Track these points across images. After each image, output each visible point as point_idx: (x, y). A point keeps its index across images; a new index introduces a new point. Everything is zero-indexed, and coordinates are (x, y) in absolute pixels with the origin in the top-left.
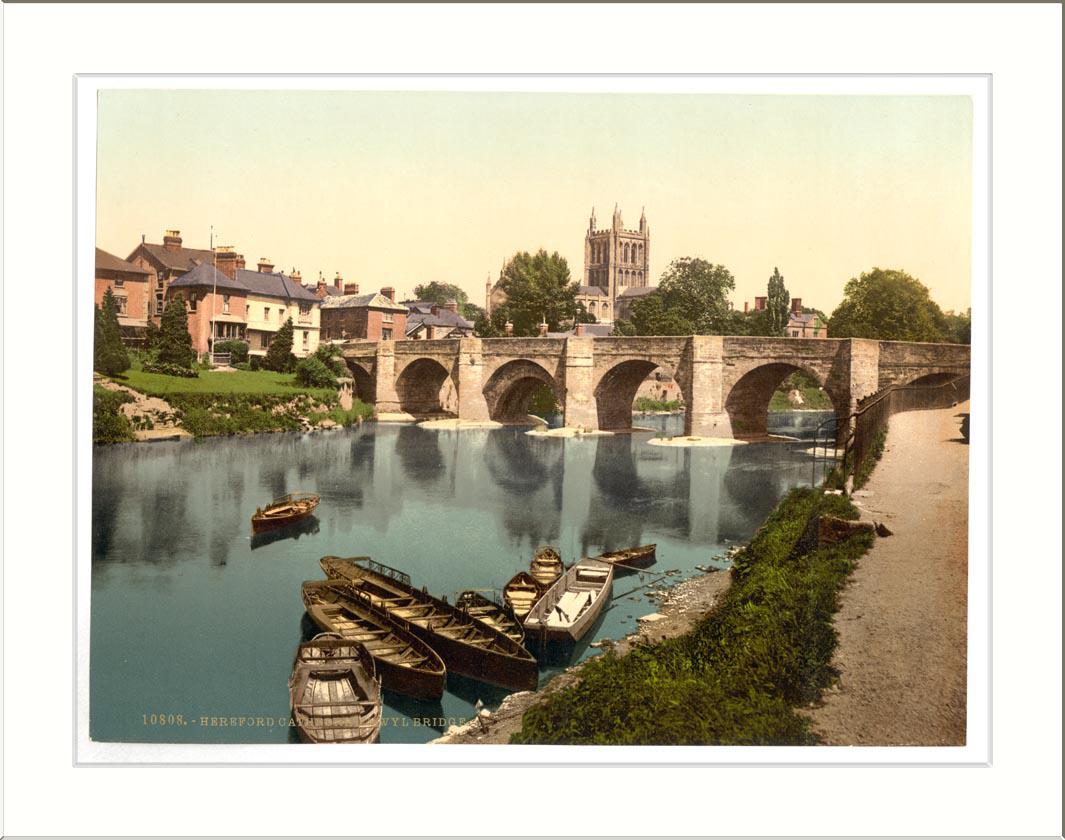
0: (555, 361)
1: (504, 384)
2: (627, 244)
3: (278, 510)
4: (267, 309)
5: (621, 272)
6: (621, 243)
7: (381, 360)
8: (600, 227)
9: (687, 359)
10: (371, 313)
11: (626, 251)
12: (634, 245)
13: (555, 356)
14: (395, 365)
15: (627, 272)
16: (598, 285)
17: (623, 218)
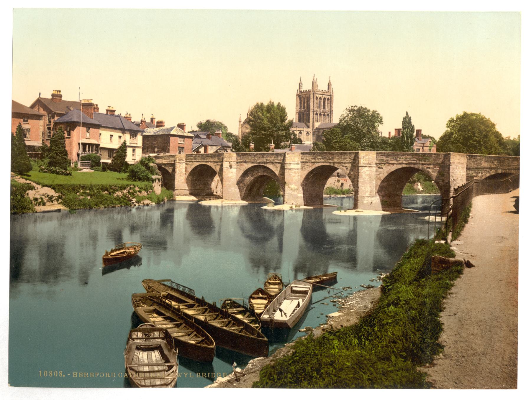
0: (279, 166)
1: (249, 179)
2: (320, 98)
4: (111, 136)
5: (317, 114)
7: (177, 165)
9: (355, 165)
11: (320, 102)
12: (325, 99)
13: (279, 163)
14: (186, 168)
15: (320, 114)
16: (303, 122)
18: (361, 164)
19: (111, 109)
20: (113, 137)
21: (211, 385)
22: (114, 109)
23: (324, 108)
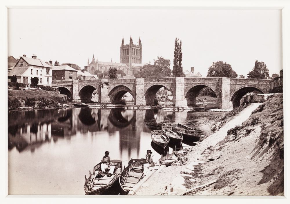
0: (132, 86)
1: (115, 92)
2: (135, 49)
3: (34, 91)
4: (37, 71)
5: (133, 58)
6: (133, 49)
7: (74, 86)
8: (125, 44)
9: (174, 85)
10: (66, 72)
11: (134, 51)
12: (137, 49)
13: (132, 84)
14: (79, 87)
15: (135, 59)
16: (125, 63)
17: (133, 41)
18: (177, 84)
19: (34, 56)
20: (38, 71)
21: (104, 186)
22: (36, 56)
23: (137, 55)
